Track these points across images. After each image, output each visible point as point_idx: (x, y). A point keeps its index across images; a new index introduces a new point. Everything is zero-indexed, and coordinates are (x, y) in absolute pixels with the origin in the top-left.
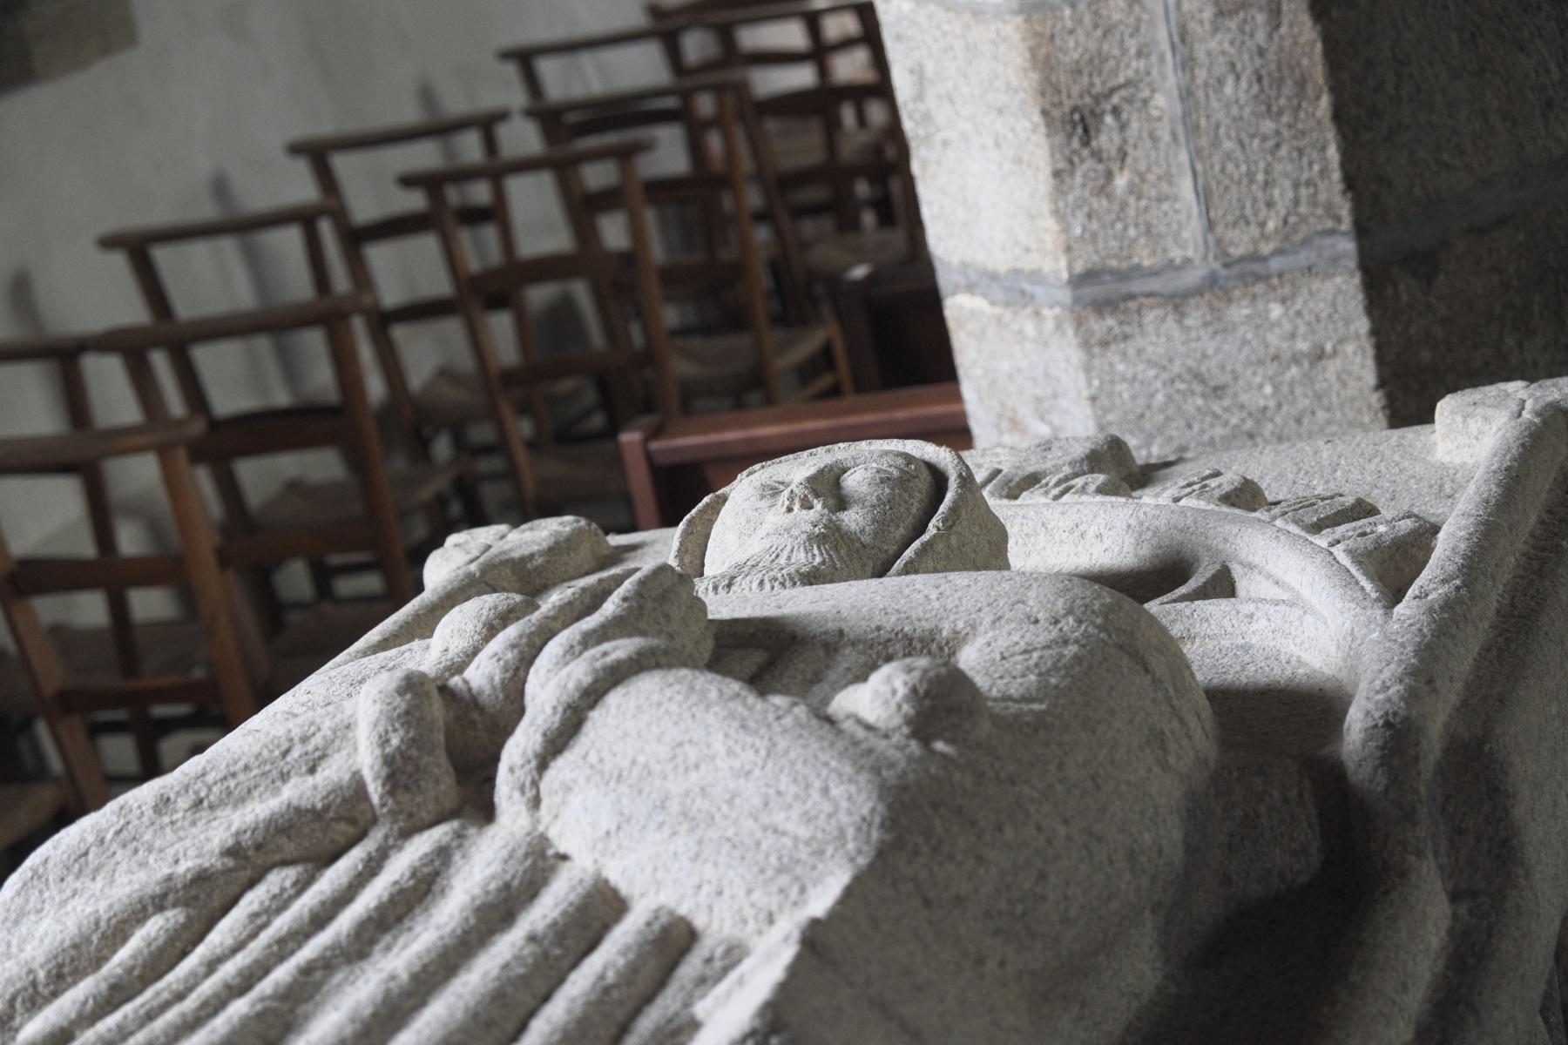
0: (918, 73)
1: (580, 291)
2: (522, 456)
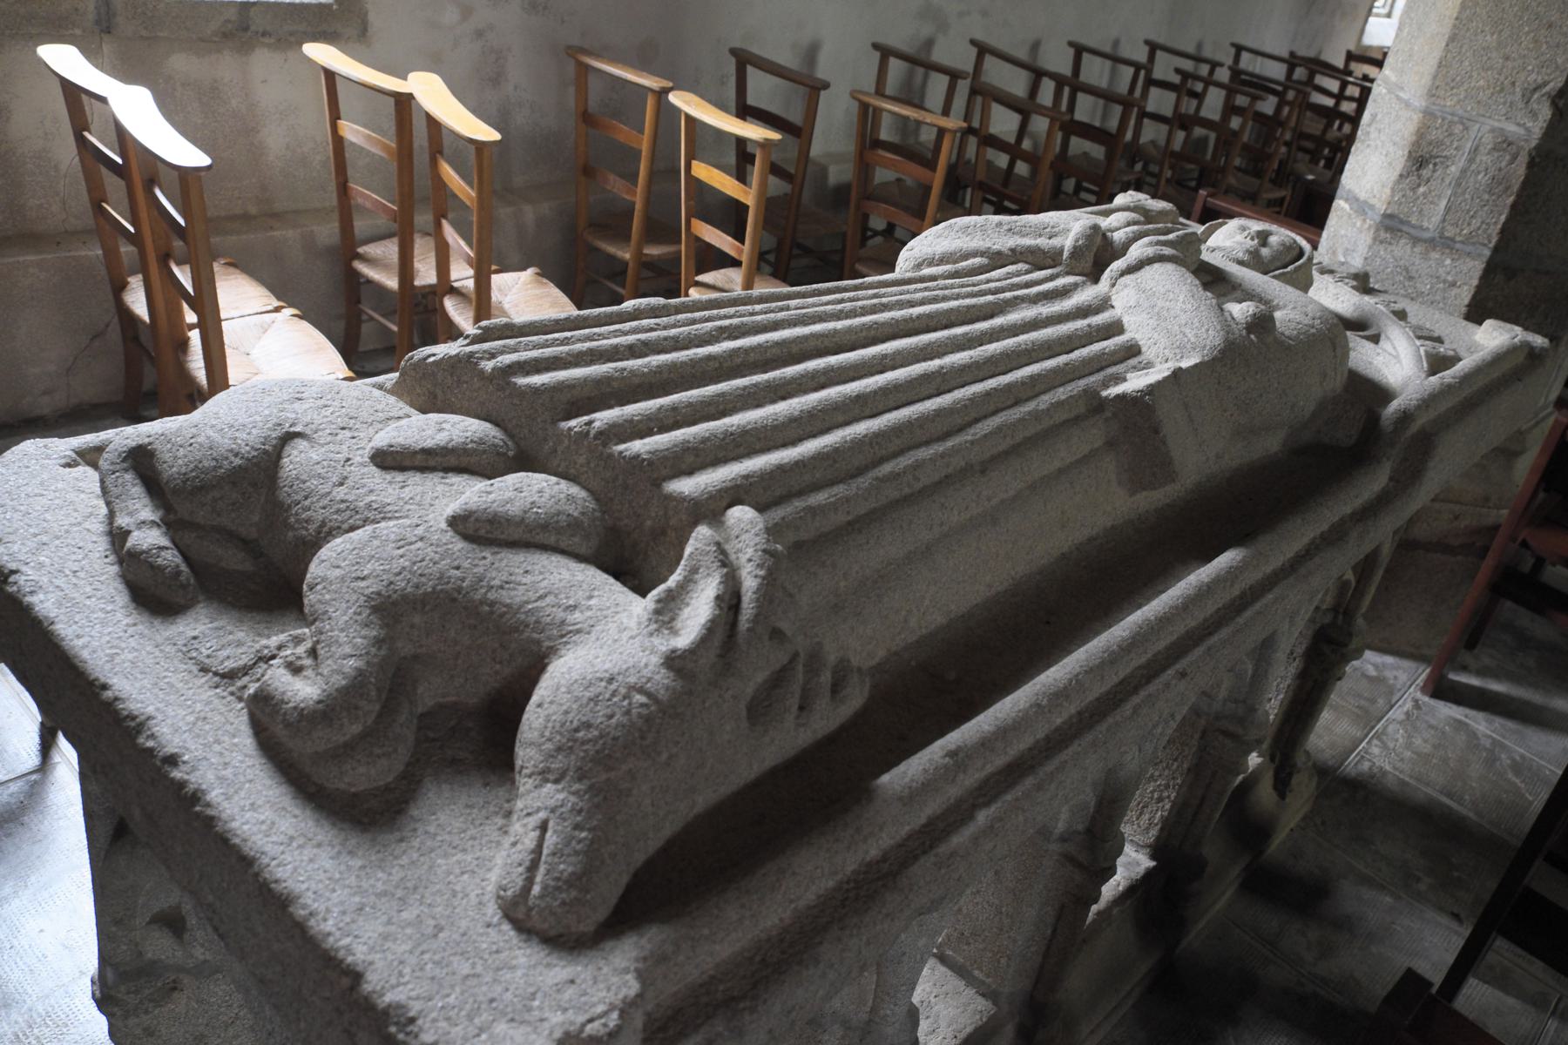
0: (1374, 116)
1: (1213, 136)
2: (1163, 182)
